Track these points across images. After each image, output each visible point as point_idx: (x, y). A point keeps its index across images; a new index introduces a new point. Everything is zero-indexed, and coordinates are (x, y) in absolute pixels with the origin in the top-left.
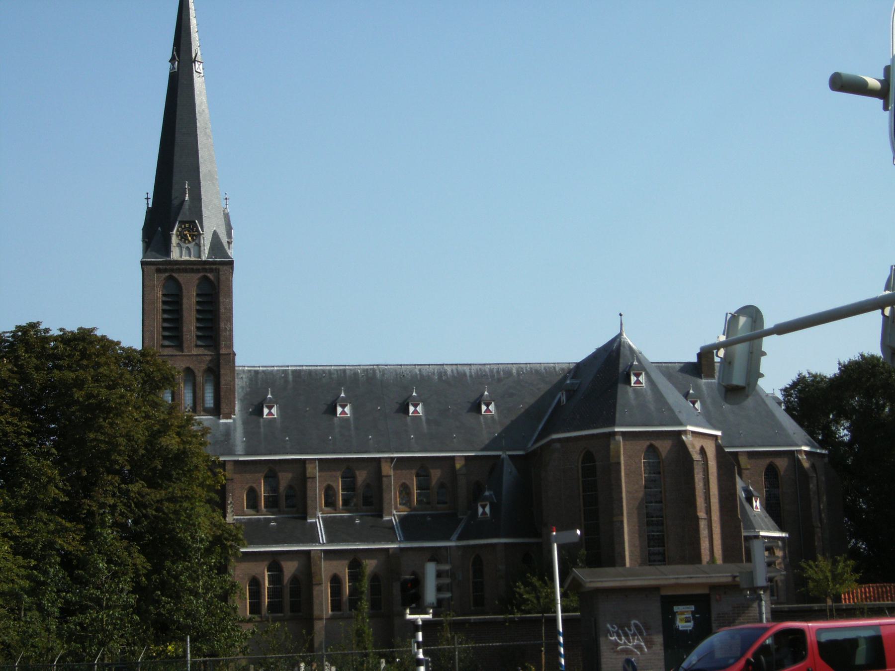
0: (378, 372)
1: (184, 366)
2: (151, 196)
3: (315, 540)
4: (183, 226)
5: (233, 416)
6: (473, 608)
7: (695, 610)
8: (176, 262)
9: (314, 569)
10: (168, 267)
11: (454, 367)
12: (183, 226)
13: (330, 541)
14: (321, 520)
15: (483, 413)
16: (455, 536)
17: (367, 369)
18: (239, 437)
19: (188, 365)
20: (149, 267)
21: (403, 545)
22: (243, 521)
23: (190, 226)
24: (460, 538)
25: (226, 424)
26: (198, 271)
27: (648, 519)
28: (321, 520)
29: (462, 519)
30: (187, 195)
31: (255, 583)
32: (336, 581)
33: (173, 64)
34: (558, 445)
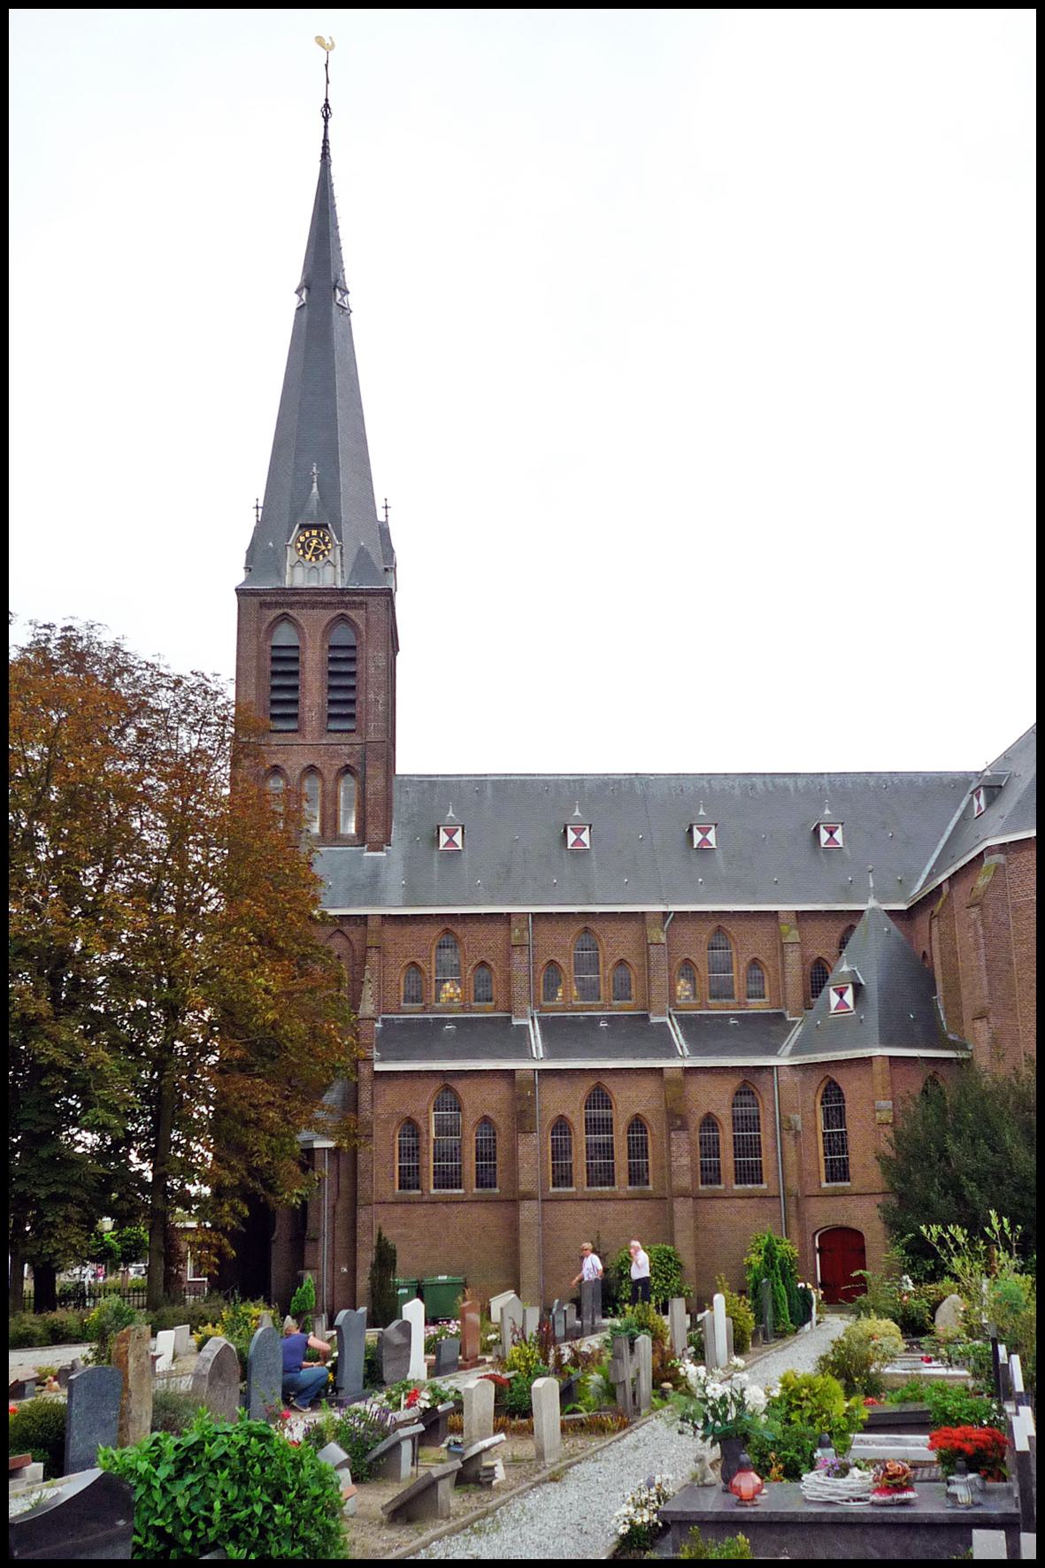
0: (637, 783)
1: (305, 764)
2: (261, 504)
3: (523, 1051)
4: (307, 534)
5: (386, 848)
6: (825, 1185)
7: (54, 1277)
8: (295, 591)
9: (907, 1521)
10: (281, 599)
11: (768, 779)
12: (307, 534)
13: (551, 1055)
14: (536, 1022)
15: (823, 846)
16: (787, 1048)
17: (620, 780)
18: (395, 877)
19: (311, 763)
20: (249, 599)
21: (687, 1064)
22: (396, 1022)
23: (318, 533)
24: (793, 1053)
25: (373, 858)
26: (326, 605)
27: (433, 1330)
28: (536, 1022)
29: (794, 1023)
30: (315, 485)
31: (411, 1127)
32: (561, 1126)
33: (300, 296)
34: (999, 858)
